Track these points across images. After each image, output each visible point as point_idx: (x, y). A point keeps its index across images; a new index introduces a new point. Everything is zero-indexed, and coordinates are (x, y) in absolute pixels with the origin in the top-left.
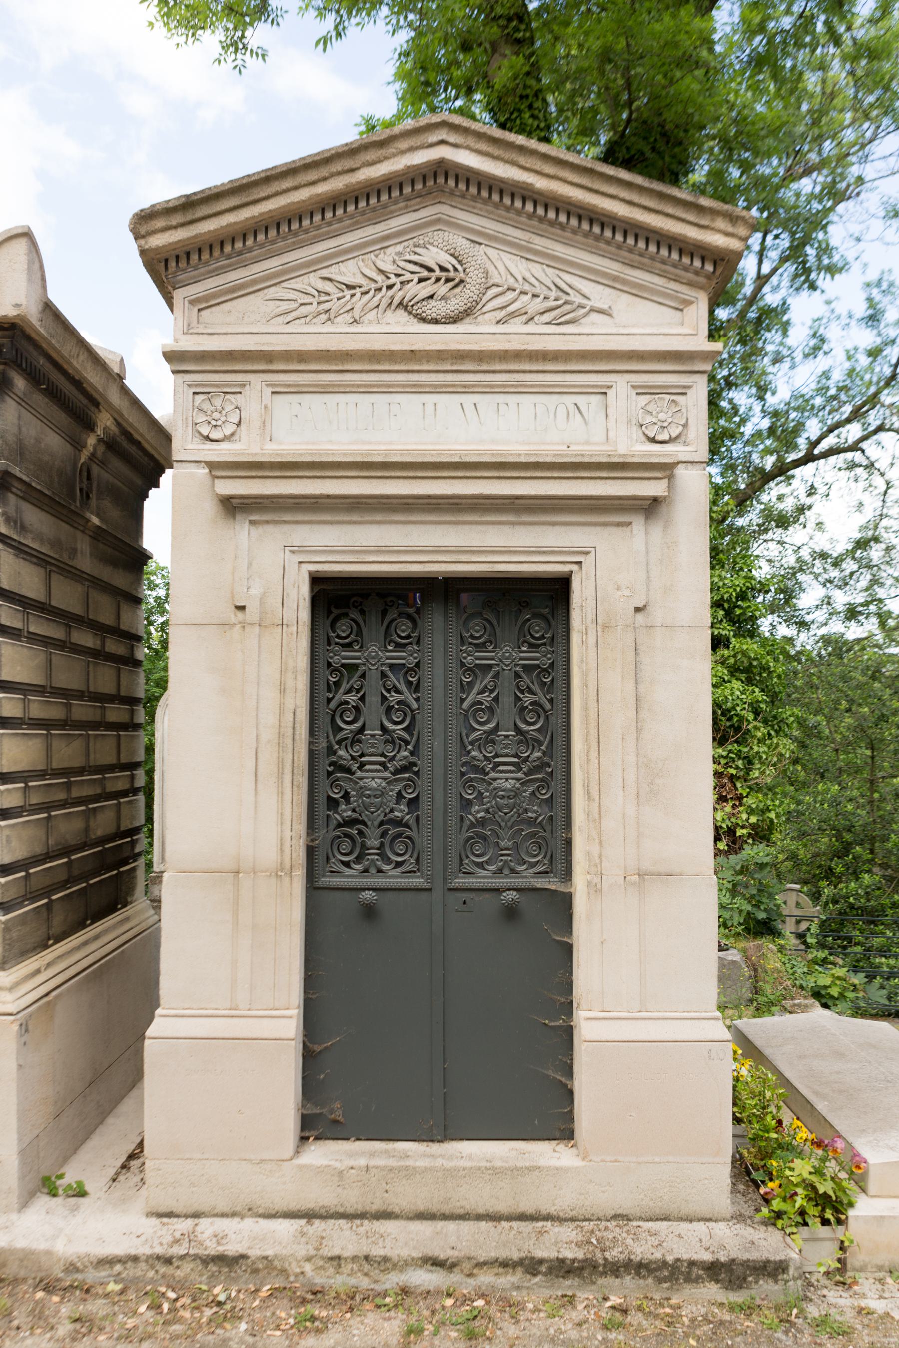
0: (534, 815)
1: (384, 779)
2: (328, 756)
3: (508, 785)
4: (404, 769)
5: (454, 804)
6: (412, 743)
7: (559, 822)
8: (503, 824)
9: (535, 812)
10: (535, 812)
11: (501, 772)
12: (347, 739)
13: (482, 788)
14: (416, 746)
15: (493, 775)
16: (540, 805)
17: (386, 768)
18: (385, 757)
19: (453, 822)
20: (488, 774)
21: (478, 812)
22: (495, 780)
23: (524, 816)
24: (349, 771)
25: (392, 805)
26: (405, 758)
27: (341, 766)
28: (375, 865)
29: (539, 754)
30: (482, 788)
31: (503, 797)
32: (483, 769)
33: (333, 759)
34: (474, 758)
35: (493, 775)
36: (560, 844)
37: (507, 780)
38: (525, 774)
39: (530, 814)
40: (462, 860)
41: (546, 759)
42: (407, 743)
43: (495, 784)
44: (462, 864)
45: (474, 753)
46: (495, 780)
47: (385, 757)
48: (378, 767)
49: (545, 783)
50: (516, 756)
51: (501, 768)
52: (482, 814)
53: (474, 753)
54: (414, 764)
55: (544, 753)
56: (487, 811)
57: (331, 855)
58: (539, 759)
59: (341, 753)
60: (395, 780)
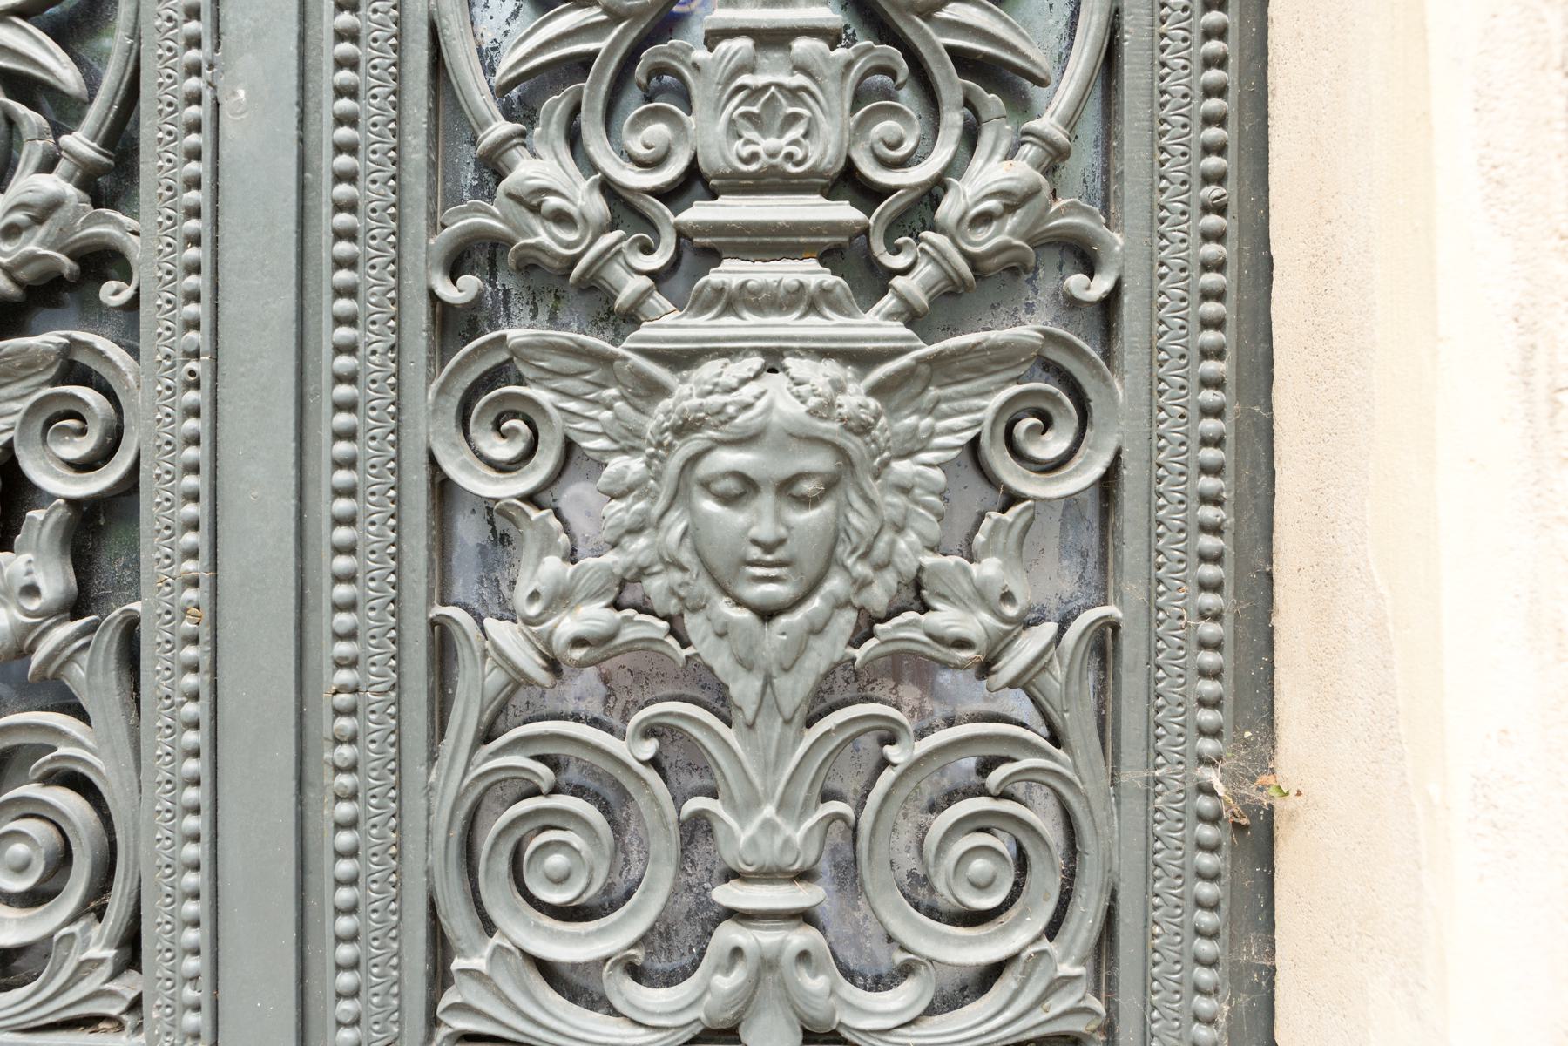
0: (975, 624)
1: (861, 359)
2: (443, 196)
3: (781, 401)
4: (986, 282)
5: (377, 536)
6: (97, 113)
7: (1172, 680)
8: (745, 689)
9: (981, 596)
10: (981, 596)
11: (731, 301)
12: (582, 63)
13: (592, 417)
14: (121, 139)
15: (670, 325)
16: (1022, 546)
17: (872, 280)
18: (869, 195)
19: (366, 665)
20: (632, 317)
21: (561, 598)
22: (682, 359)
23: (906, 628)
24: (593, 294)
25: (909, 550)
26: (46, 210)
27: (531, 264)
28: (790, 999)
29: (1021, 171)
30: (592, 417)
31: (744, 489)
32: (594, 288)
33: (489, 218)
34: (531, 201)
35: (670, 325)
36: (1193, 859)
37: (774, 360)
38: (911, 316)
39: (945, 618)
40: (440, 945)
41: (1067, 213)
42: (63, 110)
43: (685, 393)
44: (440, 978)
45: (527, 170)
46: (682, 359)
47: (869, 195)
48: (809, 273)
49: (1064, 387)
50: (847, 181)
51: (731, 273)
52: (592, 616)
53: (527, 170)
54: (102, 261)
55: (1055, 158)
56: (623, 592)
57: (459, 922)
58: (1013, 200)
59: (540, 166)
60: (941, 367)
